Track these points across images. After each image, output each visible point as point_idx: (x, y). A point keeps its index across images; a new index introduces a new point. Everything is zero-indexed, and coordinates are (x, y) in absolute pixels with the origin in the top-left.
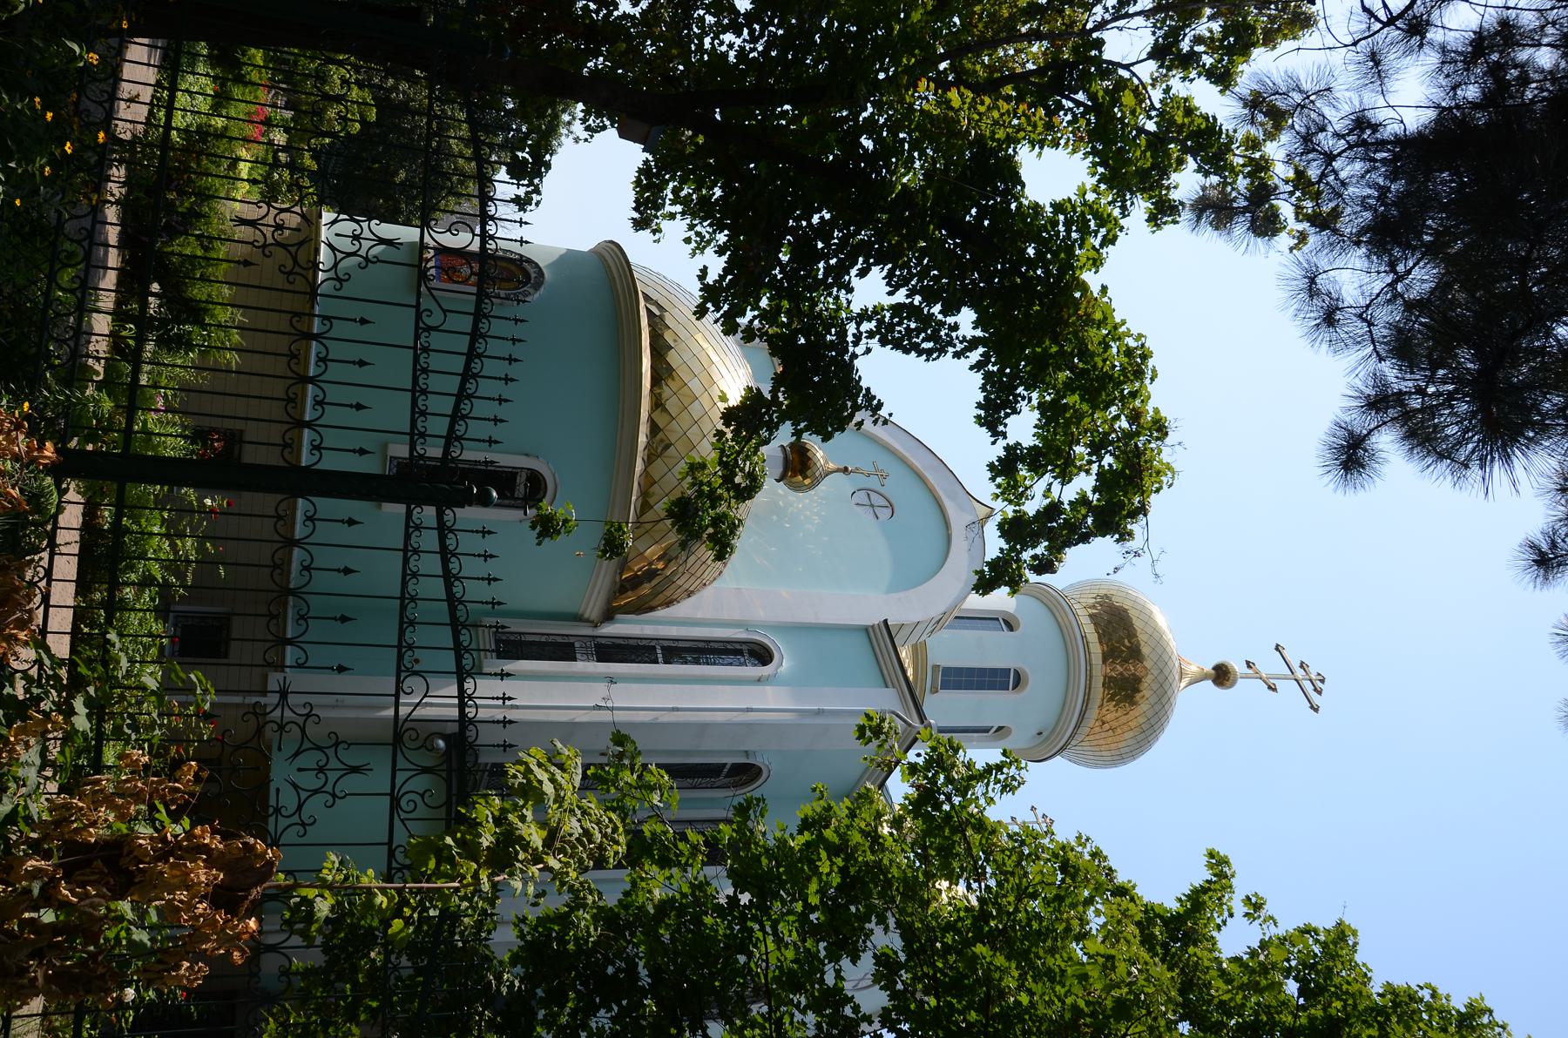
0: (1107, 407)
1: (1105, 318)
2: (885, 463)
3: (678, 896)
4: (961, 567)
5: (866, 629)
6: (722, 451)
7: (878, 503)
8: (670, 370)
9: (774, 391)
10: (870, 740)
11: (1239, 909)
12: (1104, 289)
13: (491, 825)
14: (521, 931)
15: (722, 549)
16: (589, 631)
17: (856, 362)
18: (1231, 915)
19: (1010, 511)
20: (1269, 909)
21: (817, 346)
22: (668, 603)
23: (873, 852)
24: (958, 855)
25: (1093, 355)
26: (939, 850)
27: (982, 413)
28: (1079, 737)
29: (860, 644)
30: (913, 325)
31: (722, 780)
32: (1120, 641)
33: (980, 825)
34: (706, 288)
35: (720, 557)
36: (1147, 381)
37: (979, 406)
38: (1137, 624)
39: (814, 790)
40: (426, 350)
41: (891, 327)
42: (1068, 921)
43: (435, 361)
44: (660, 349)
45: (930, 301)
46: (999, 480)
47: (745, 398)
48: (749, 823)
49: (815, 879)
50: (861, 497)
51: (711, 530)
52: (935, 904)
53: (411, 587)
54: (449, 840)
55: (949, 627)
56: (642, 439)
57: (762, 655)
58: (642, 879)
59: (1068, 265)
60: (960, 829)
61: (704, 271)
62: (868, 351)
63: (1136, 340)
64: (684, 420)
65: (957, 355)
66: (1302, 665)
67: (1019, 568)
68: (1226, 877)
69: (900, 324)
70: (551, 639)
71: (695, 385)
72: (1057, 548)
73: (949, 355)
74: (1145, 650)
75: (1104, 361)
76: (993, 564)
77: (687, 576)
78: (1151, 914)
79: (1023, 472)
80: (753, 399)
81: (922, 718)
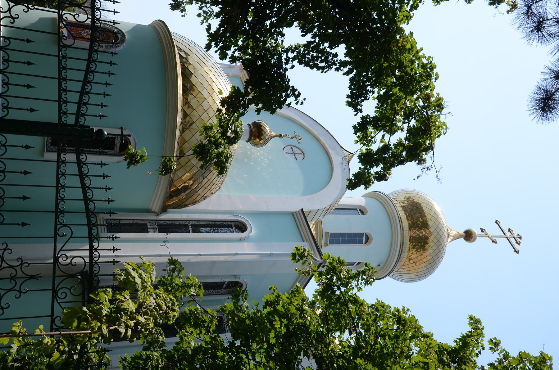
0: (412, 95)
1: (412, 47)
2: (300, 132)
3: (204, 344)
4: (339, 180)
5: (292, 214)
6: (220, 120)
7: (298, 152)
8: (192, 85)
9: (246, 88)
10: (298, 260)
11: (487, 346)
12: (411, 34)
13: (108, 303)
14: (124, 365)
15: (222, 169)
16: (154, 218)
17: (287, 73)
18: (483, 349)
19: (364, 149)
20: (503, 346)
21: (267, 66)
22: (194, 203)
23: (301, 318)
24: (344, 317)
25: (406, 67)
26: (335, 315)
27: (350, 100)
28: (398, 267)
29: (290, 222)
30: (315, 55)
31: (223, 290)
32: (417, 219)
33: (355, 301)
34: (210, 35)
35: (221, 173)
36: (433, 80)
37: (348, 96)
38: (426, 210)
39: (270, 289)
40: (65, 57)
41: (304, 56)
42: (402, 348)
43: (70, 63)
44: (187, 75)
45: (322, 41)
46: (358, 134)
47: (232, 92)
48: (240, 304)
49: (273, 331)
50: (288, 149)
51: (215, 160)
52: (332, 345)
53: (61, 181)
54: (85, 309)
55: (333, 213)
56: (179, 120)
57: (241, 227)
58: (185, 336)
59: (393, 22)
60: (345, 304)
61: (209, 26)
62: (293, 67)
63: (427, 60)
64: (200, 110)
65: (337, 69)
66: (509, 230)
67: (369, 177)
68: (479, 329)
69: (308, 54)
70: (135, 222)
71: (204, 92)
72: (388, 168)
73: (333, 69)
74: (430, 223)
75: (412, 70)
76: (355, 176)
77: (203, 189)
78: (441, 349)
79: (370, 129)
80: (236, 94)
81: (321, 255)
